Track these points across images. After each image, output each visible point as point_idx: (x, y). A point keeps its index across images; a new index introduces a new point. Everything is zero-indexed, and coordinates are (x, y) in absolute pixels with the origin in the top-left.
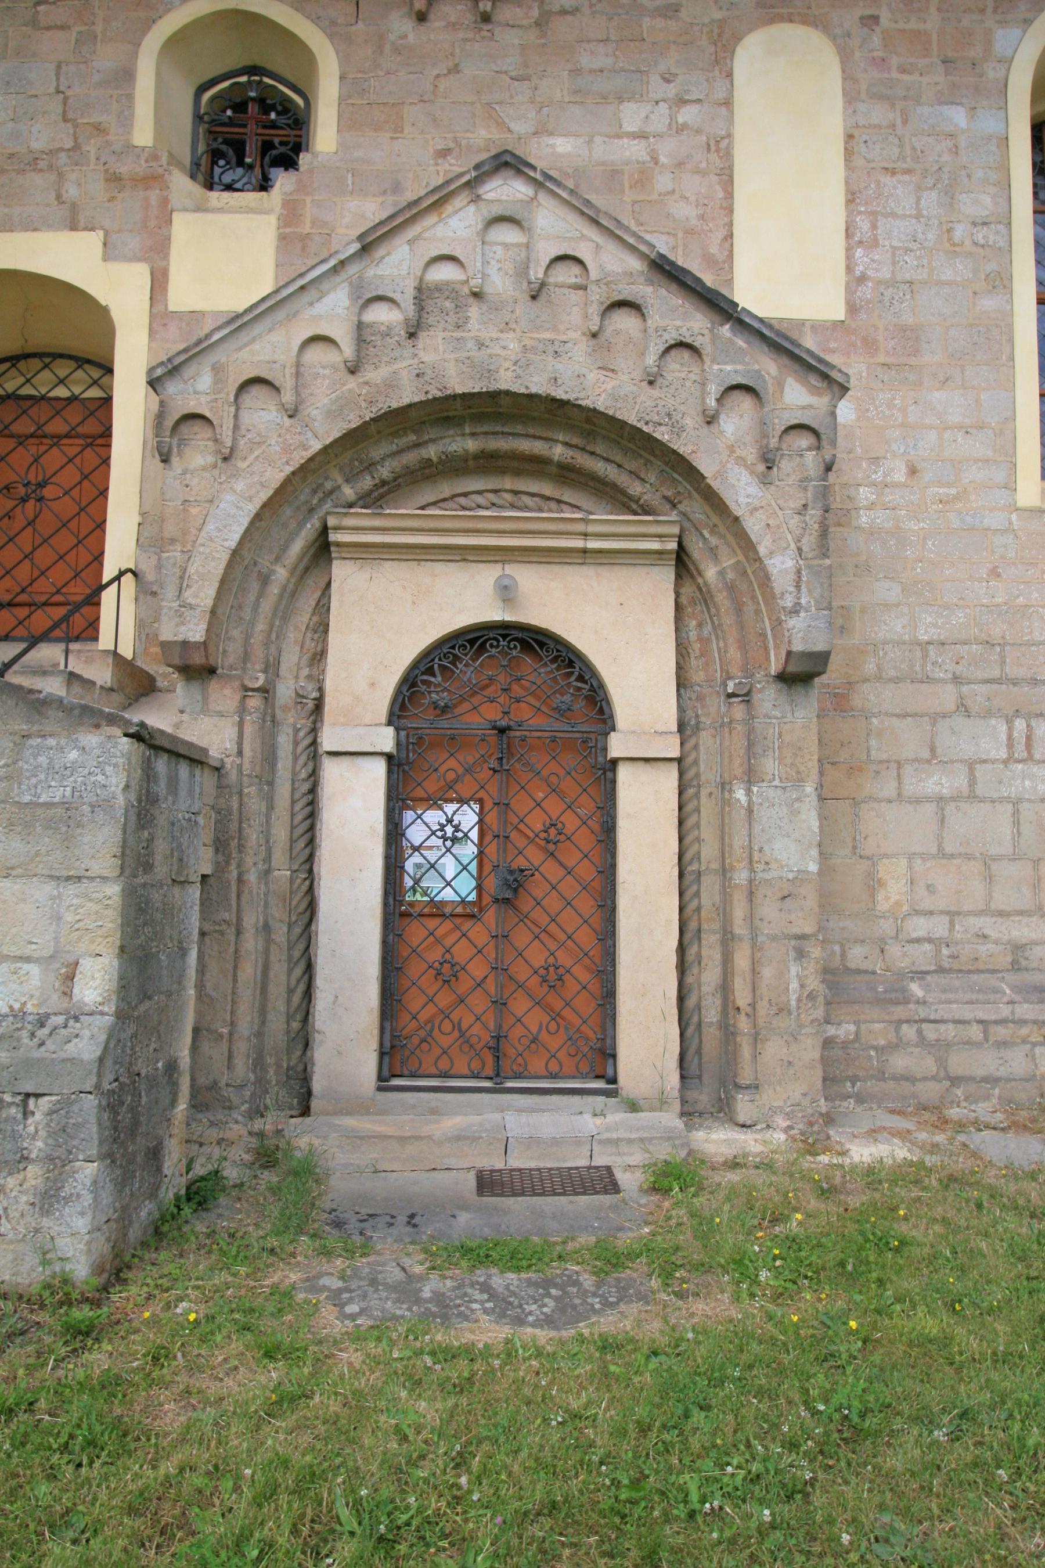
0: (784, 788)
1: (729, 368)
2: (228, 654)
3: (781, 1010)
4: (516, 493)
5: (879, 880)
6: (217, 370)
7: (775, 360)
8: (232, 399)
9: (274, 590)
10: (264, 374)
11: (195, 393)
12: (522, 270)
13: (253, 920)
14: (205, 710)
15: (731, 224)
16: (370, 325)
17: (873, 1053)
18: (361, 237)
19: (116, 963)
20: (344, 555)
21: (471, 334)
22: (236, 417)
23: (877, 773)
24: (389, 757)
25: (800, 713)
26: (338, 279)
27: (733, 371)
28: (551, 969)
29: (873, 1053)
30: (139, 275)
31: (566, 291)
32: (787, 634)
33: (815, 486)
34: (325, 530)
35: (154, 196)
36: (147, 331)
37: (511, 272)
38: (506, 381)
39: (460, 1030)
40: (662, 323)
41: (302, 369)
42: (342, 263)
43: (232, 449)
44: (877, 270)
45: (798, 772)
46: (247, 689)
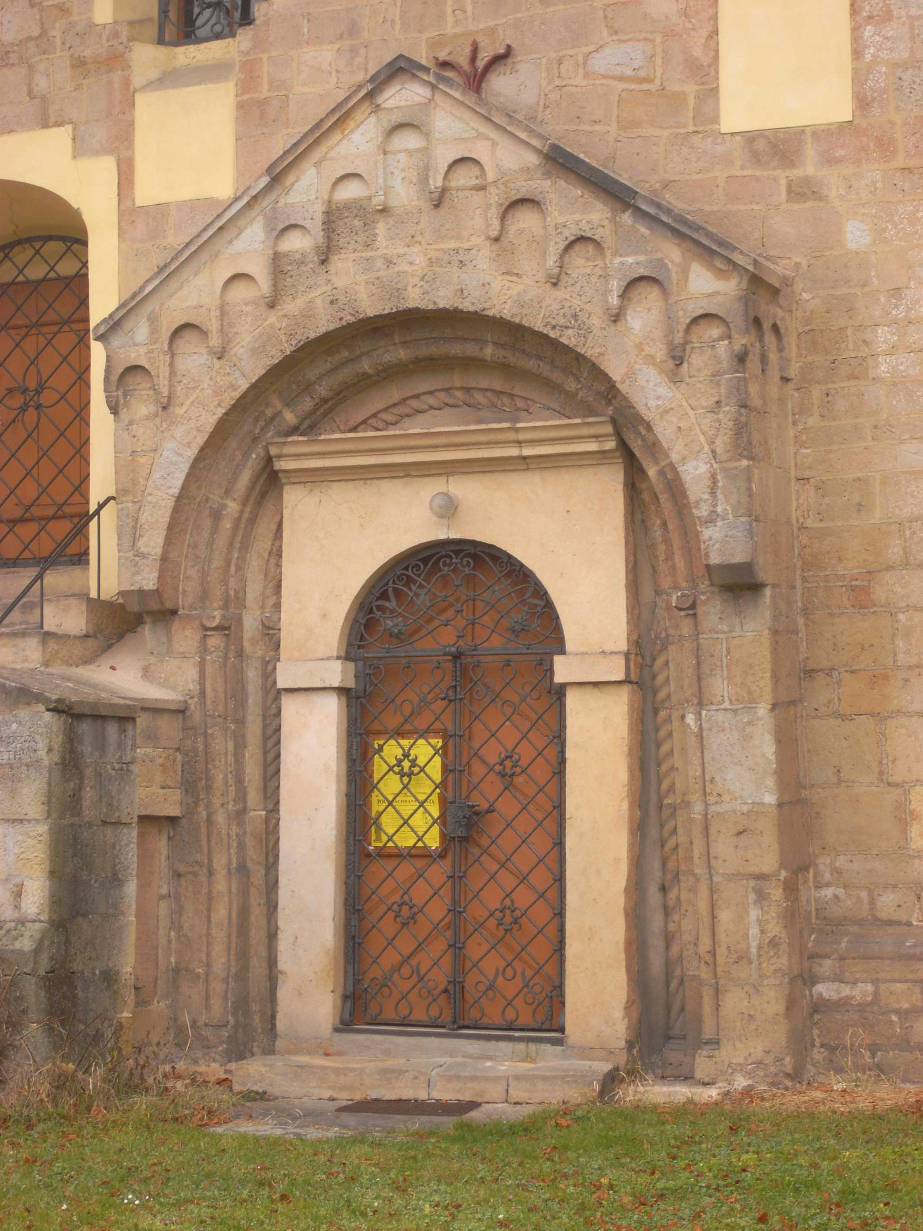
0: (735, 711)
1: (630, 260)
2: (186, 594)
3: (740, 958)
4: (468, 390)
5: (912, 812)
6: (153, 320)
7: (679, 245)
8: (166, 347)
9: (227, 525)
10: (192, 320)
11: (135, 345)
12: (424, 179)
13: (224, 861)
14: (170, 652)
15: (715, 18)
16: (286, 255)
17: (894, 1018)
18: (269, 170)
19: (48, 883)
20: (292, 480)
21: (379, 253)
22: (171, 364)
23: (906, 681)
24: (342, 691)
25: (750, 626)
26: (254, 213)
27: (633, 262)
28: (508, 912)
29: (894, 1018)
30: (105, 169)
31: (468, 193)
32: (703, 546)
33: (730, 380)
34: (269, 460)
35: (116, 77)
36: (116, 232)
37: (414, 180)
38: (414, 299)
39: (418, 975)
40: (561, 220)
41: (227, 308)
42: (255, 198)
43: (169, 398)
44: (891, 50)
45: (750, 693)
46: (206, 629)
